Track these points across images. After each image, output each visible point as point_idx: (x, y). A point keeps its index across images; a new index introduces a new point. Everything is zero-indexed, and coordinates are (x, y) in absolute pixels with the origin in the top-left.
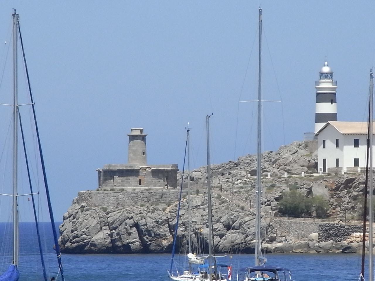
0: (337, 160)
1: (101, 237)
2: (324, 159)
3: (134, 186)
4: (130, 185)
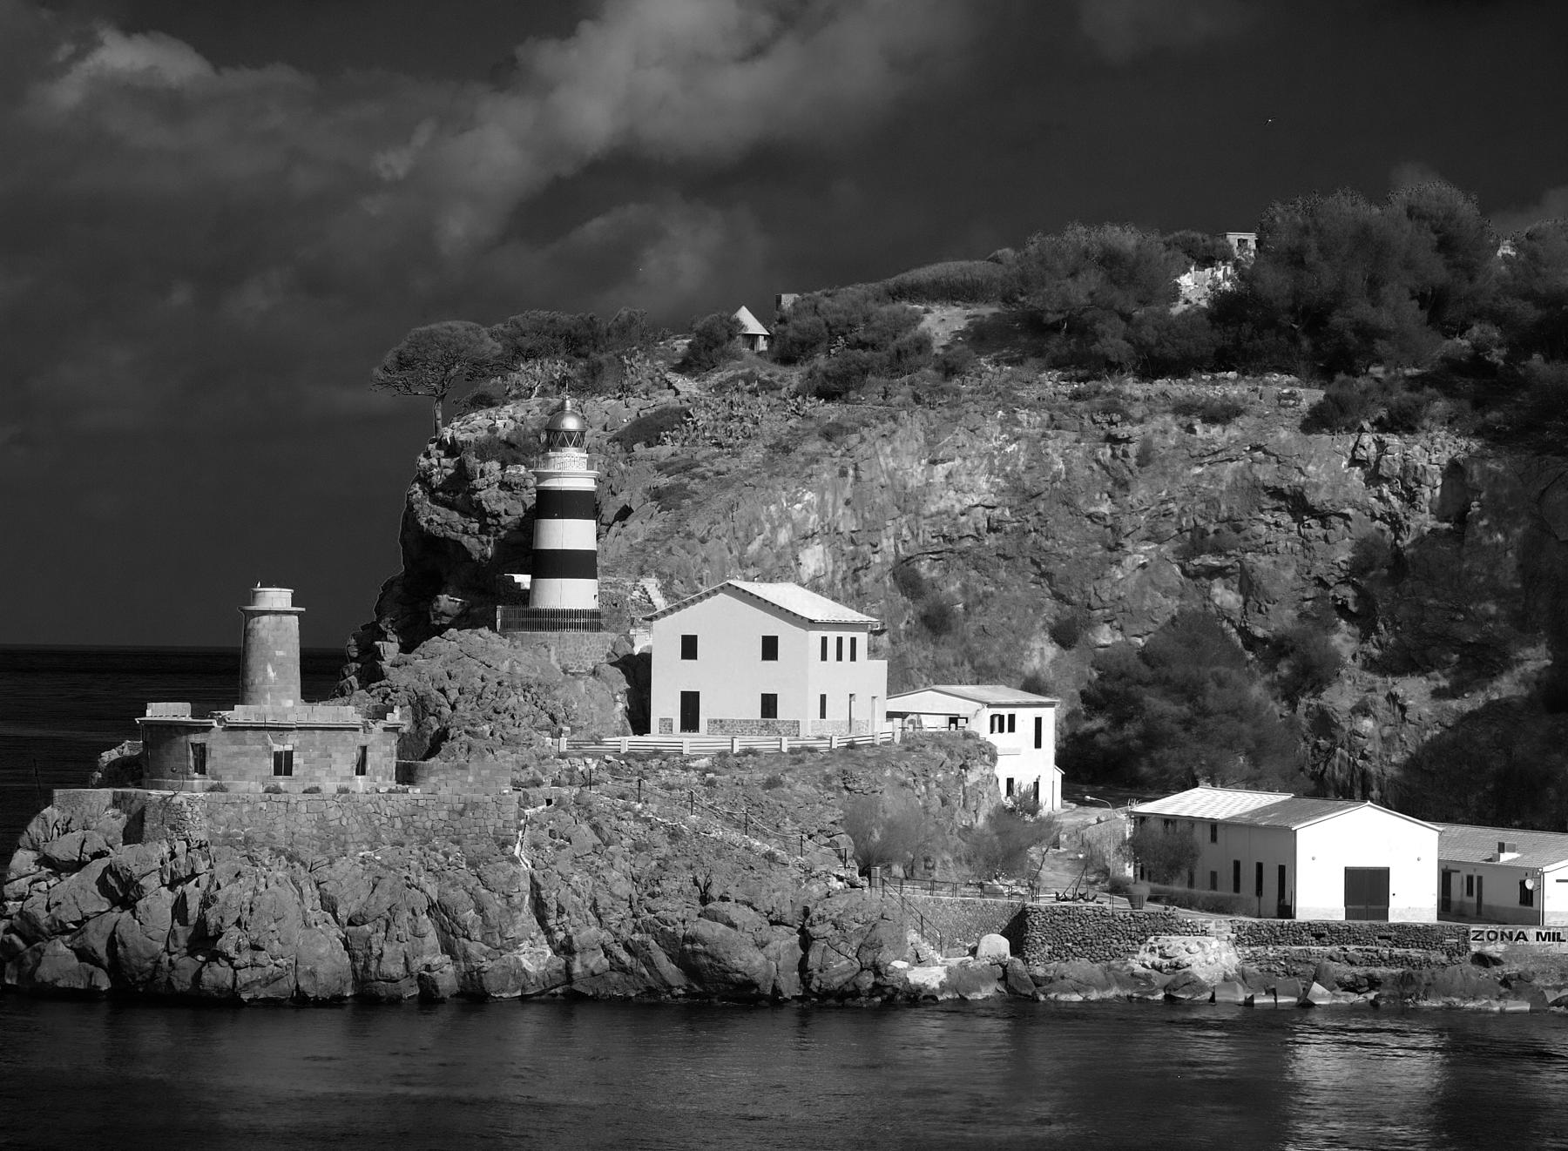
0: (823, 698)
1: (323, 957)
2: (694, 657)
3: (343, 779)
4: (331, 774)
